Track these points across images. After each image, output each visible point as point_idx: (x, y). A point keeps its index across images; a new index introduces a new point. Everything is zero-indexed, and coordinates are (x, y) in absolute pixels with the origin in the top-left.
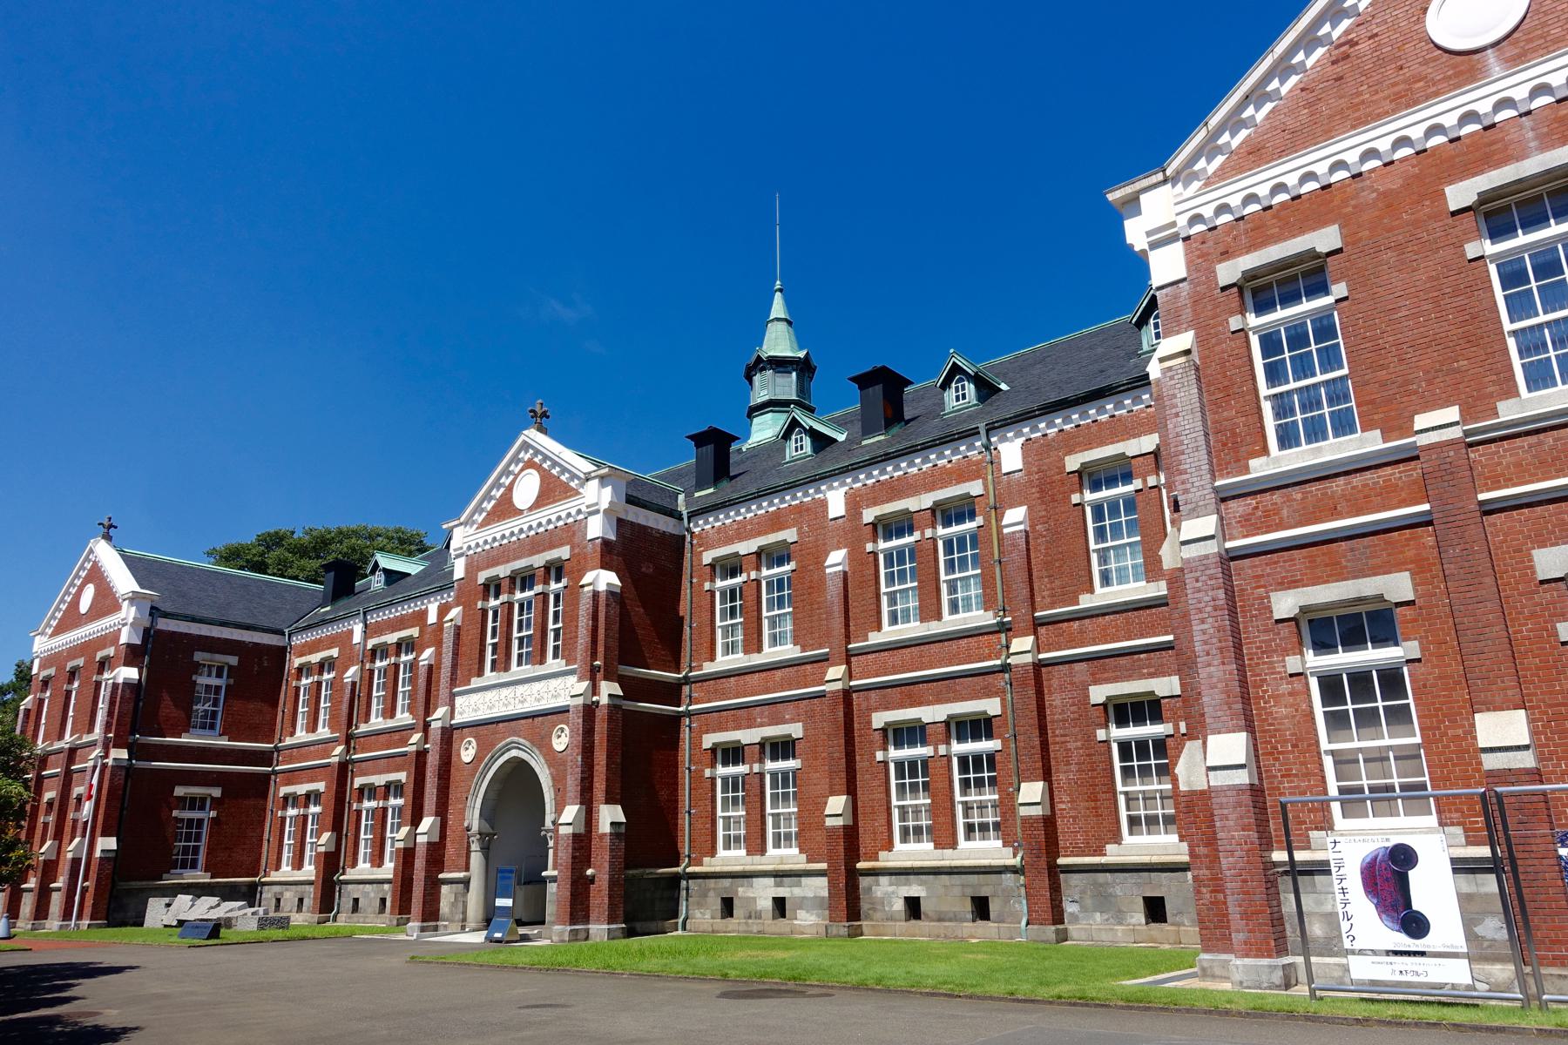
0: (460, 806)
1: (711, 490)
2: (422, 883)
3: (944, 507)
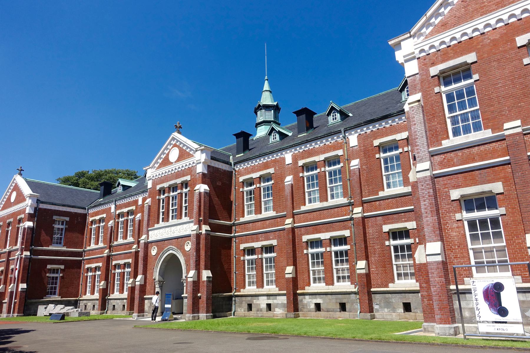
0: (152, 271)
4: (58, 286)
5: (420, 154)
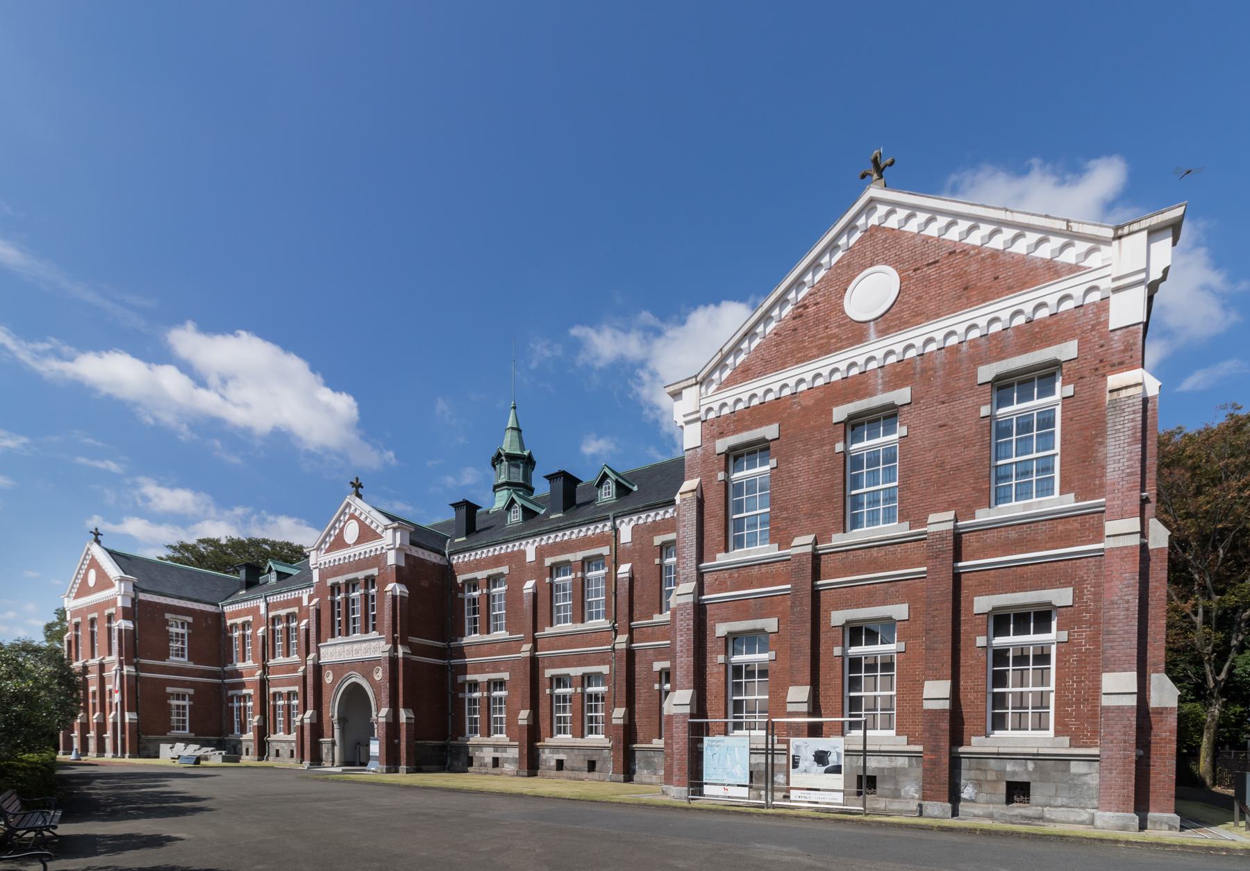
1: (561, 515)
2: (309, 743)
3: (590, 560)
4: (187, 718)
5: (685, 571)
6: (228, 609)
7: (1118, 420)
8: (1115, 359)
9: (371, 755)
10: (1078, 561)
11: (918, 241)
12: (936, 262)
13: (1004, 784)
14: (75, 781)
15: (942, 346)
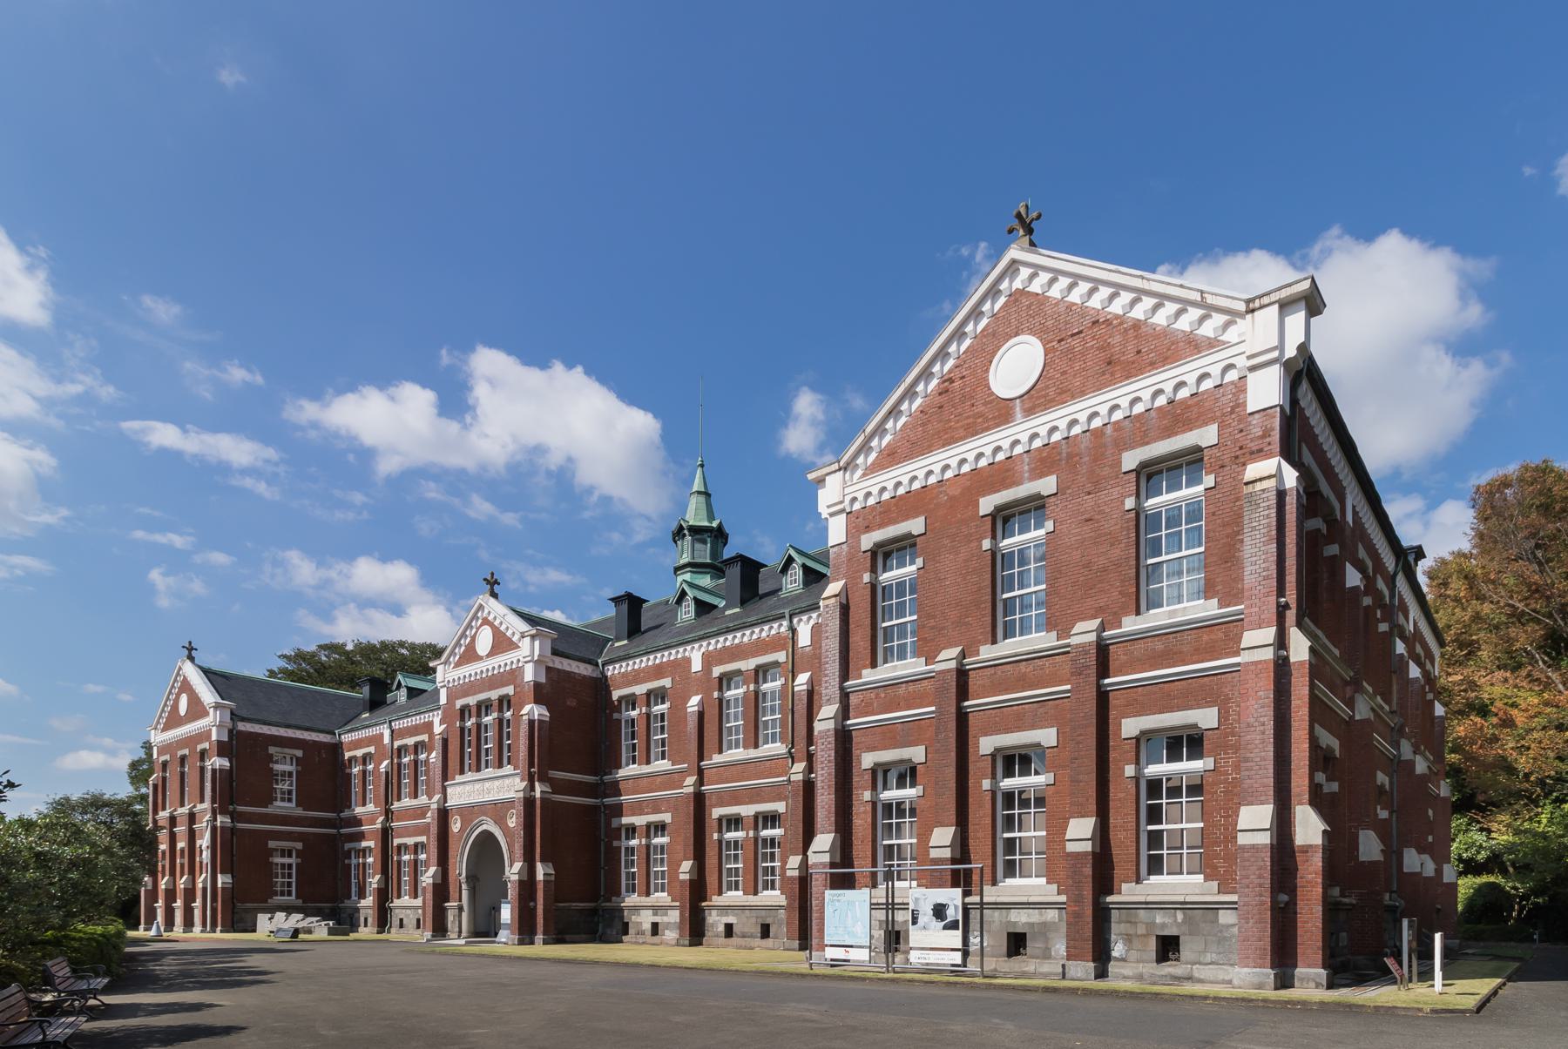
1: (737, 610)
3: (764, 668)
6: (346, 738)
7: (1254, 516)
8: (1254, 446)
9: (502, 922)
10: (1223, 676)
11: (1062, 308)
12: (1081, 332)
13: (1155, 938)
14: (144, 958)
15: (1086, 429)
